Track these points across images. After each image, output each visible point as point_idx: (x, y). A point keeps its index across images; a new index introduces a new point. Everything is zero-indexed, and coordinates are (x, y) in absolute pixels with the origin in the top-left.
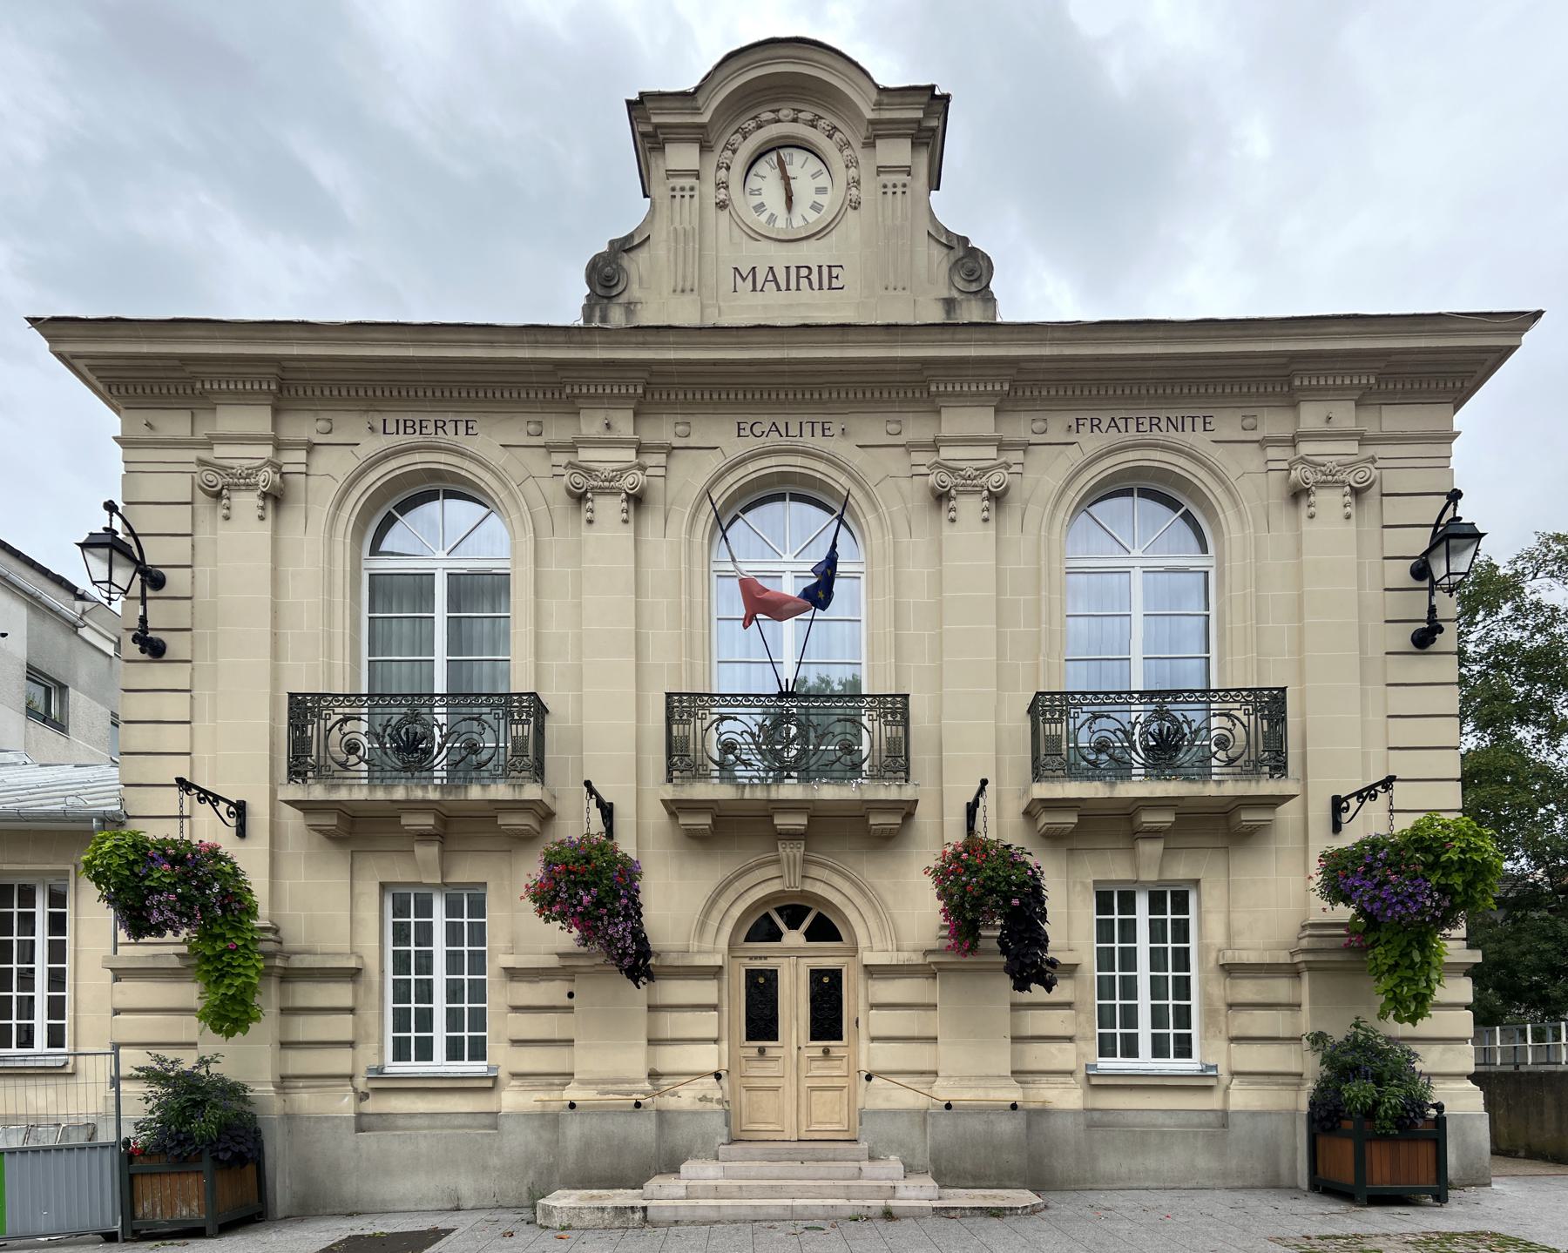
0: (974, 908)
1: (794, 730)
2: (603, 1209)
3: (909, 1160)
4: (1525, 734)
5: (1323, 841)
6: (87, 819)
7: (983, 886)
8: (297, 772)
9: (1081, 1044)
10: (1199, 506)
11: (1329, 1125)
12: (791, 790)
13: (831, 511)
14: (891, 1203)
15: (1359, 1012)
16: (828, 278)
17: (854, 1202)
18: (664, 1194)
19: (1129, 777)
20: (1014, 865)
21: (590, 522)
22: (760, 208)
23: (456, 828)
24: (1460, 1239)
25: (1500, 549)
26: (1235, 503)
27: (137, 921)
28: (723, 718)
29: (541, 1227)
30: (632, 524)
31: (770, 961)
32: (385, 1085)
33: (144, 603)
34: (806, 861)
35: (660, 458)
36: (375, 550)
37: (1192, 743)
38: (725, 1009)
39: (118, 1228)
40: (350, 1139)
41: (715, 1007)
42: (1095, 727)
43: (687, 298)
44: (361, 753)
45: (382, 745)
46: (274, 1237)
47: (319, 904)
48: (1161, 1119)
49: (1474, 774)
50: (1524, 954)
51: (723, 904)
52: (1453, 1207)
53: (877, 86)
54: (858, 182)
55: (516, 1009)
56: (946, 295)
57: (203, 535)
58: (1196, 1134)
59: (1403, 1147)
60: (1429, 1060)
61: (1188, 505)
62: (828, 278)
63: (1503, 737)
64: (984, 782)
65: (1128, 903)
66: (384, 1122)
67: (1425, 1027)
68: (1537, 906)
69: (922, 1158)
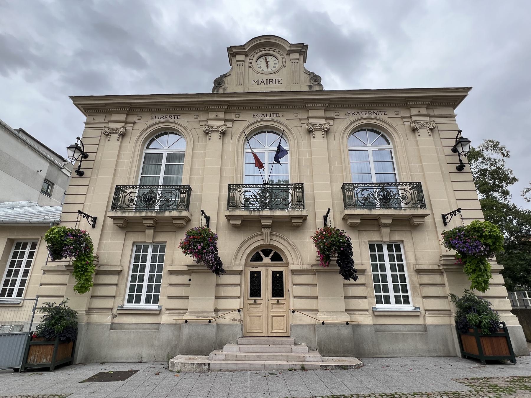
0: (328, 251)
1: (268, 194)
2: (194, 364)
3: (309, 345)
4: (496, 195)
5: (441, 229)
6: (49, 223)
7: (331, 243)
8: (114, 208)
9: (370, 299)
10: (386, 133)
11: (465, 331)
12: (266, 212)
13: (279, 135)
14: (304, 363)
15: (463, 288)
16: (278, 82)
17: (290, 363)
18: (217, 358)
19: (376, 208)
20: (341, 236)
21: (209, 139)
22: (260, 67)
23: (160, 225)
24: (526, 380)
25: (475, 145)
27: (56, 254)
28: (246, 191)
29: (170, 371)
31: (258, 268)
32: (123, 312)
33: (81, 162)
34: (271, 235)
35: (231, 123)
36: (147, 148)
37: (394, 198)
38: (243, 285)
39: (20, 367)
40: (107, 333)
41: (239, 285)
42: (363, 193)
43: (240, 86)
45: (141, 200)
46: (73, 372)
47: (113, 249)
48: (402, 328)
49: (486, 206)
50: (515, 265)
51: (243, 249)
52: (518, 365)
55: (171, 285)
57: (101, 144)
58: (416, 334)
59: (494, 339)
60: (495, 305)
61: (382, 133)
62: (278, 82)
63: (489, 196)
64: (329, 210)
65: (380, 249)
66: (121, 326)
67: (488, 293)
68: (516, 249)
69: (315, 345)
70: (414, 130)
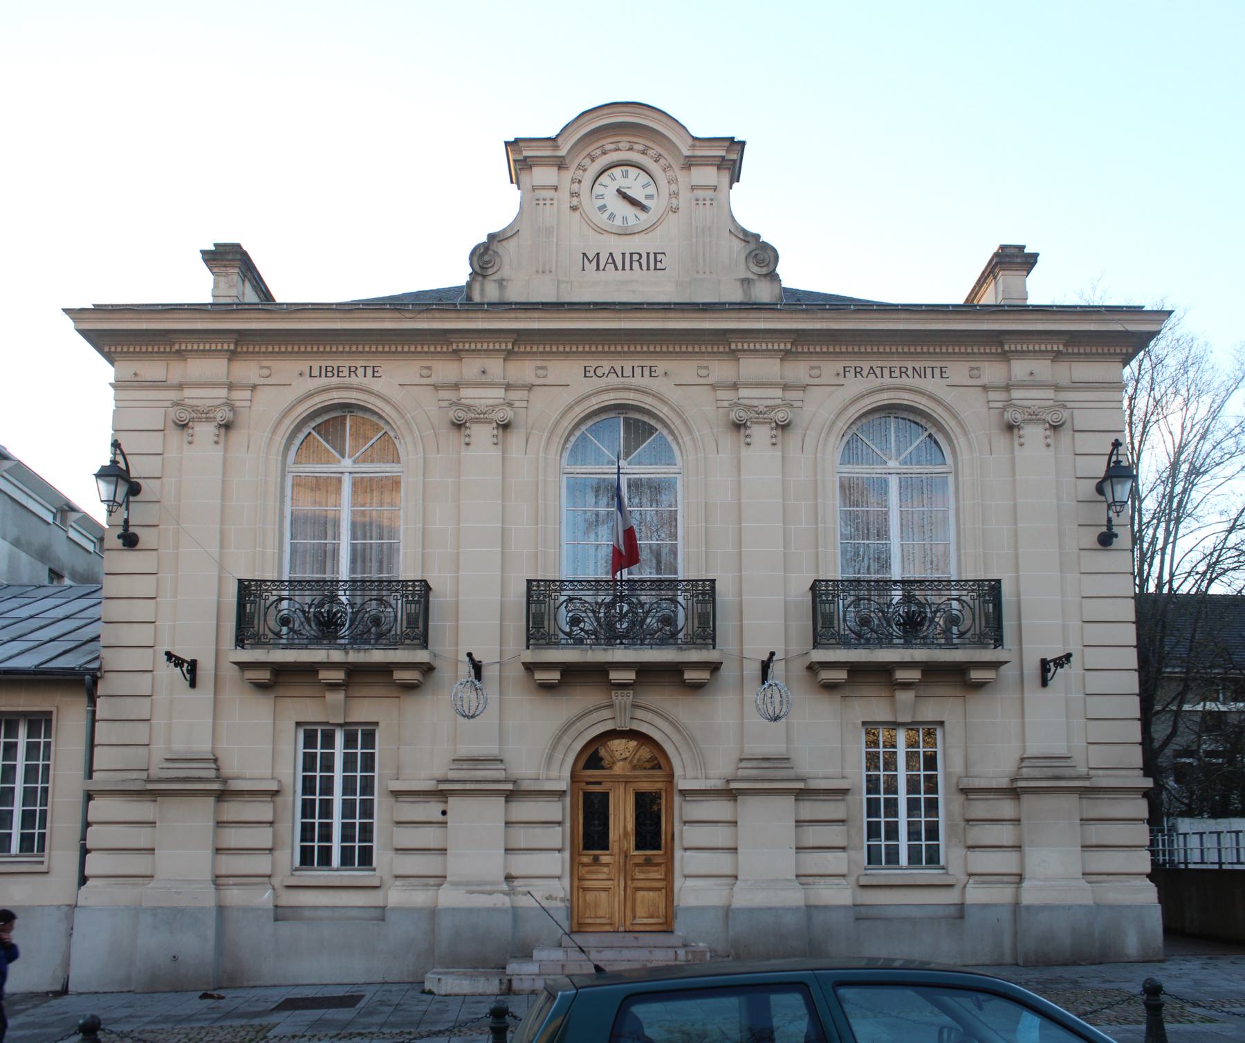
1: (626, 608)
8: (240, 642)
9: (852, 853)
22: (603, 208)
26: (965, 433)
30: (500, 446)
35: (523, 394)
51: (567, 740)
56: (743, 276)
62: (654, 261)
70: (1010, 428)
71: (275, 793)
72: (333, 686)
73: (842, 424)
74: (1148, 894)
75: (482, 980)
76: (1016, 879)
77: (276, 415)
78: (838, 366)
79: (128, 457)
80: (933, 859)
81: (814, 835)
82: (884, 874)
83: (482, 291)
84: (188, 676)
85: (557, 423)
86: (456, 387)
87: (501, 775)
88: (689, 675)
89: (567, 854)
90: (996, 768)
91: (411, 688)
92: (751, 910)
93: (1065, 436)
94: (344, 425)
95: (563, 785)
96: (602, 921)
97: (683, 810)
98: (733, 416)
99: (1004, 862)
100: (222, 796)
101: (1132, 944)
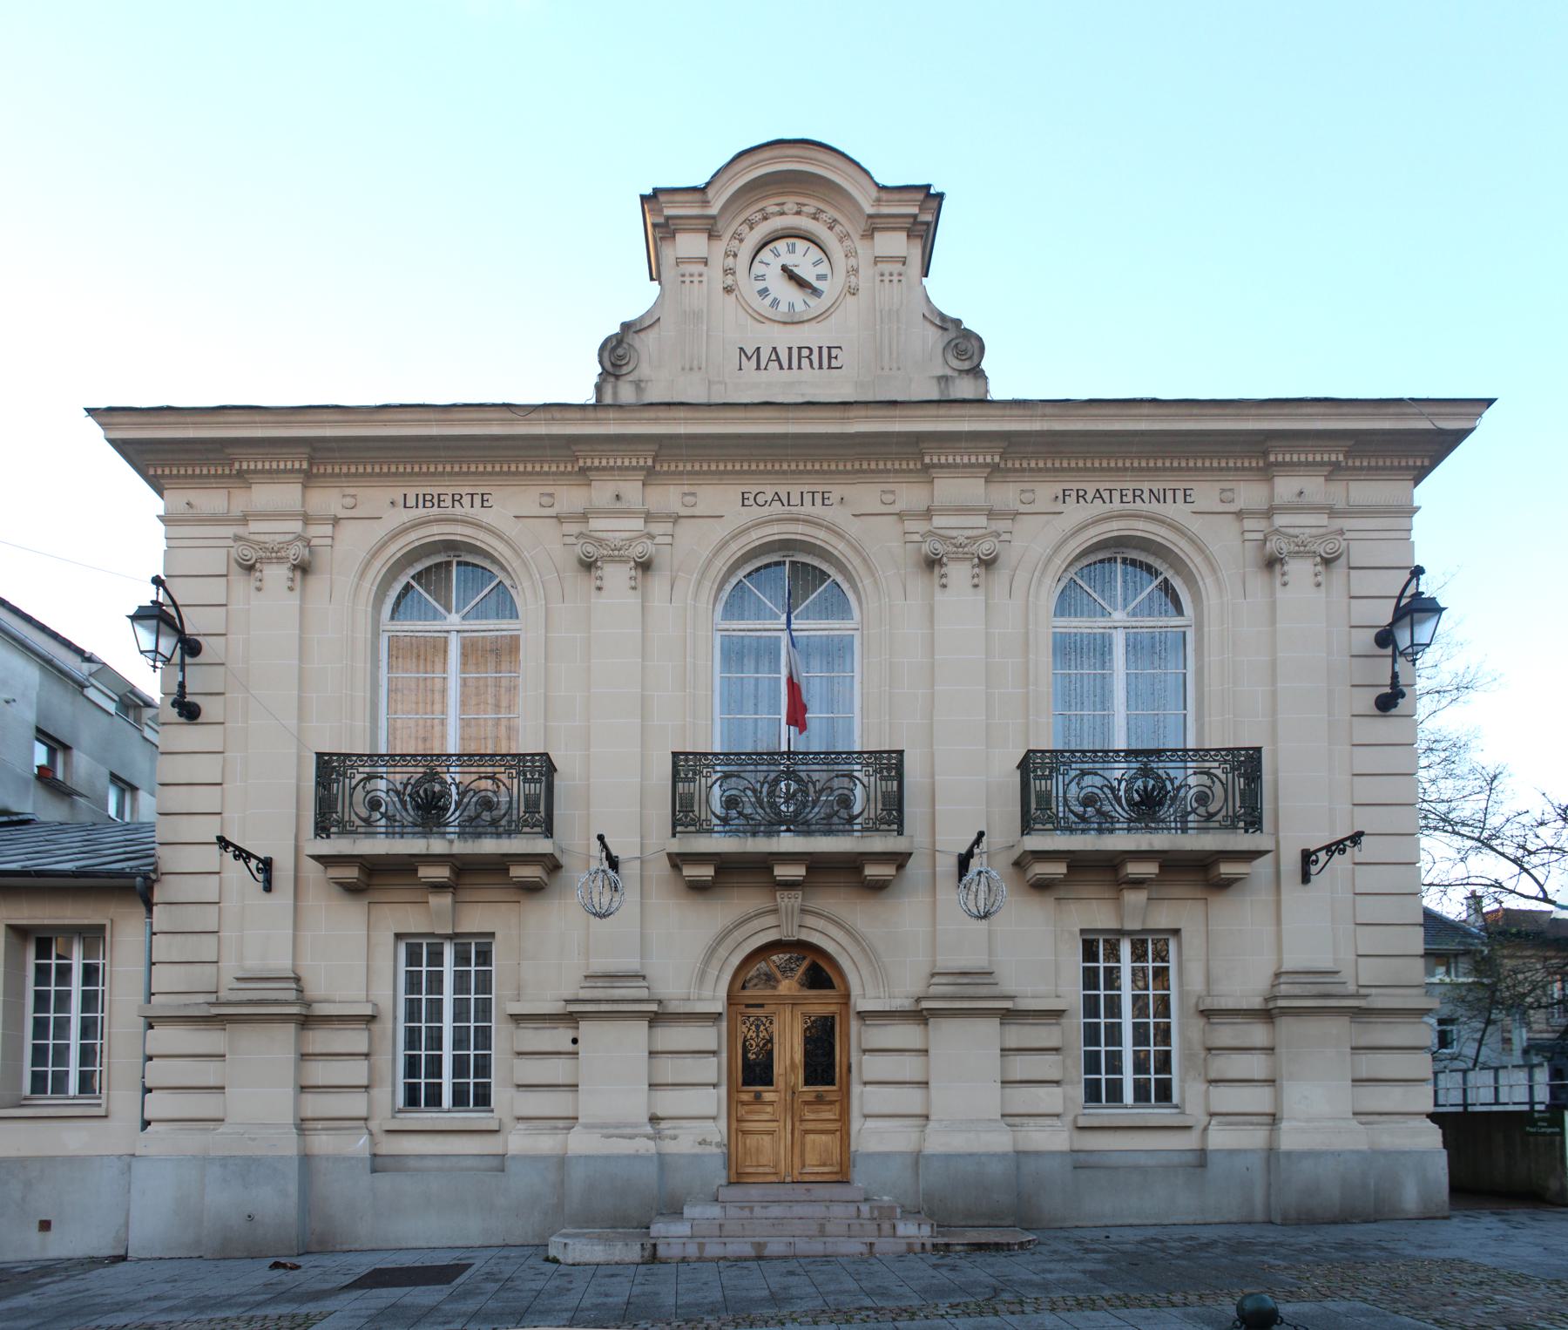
8: (322, 829)
22: (764, 292)
26: (1214, 570)
30: (639, 592)
33: (183, 670)
35: (666, 527)
44: (383, 809)
51: (722, 952)
53: (877, 184)
54: (857, 271)
62: (827, 357)
64: (981, 834)
71: (371, 1019)
72: (438, 887)
73: (1060, 562)
74: (1432, 1137)
75: (620, 1245)
76: (1268, 1119)
77: (362, 555)
78: (1057, 489)
79: (183, 610)
80: (1164, 1092)
81: (1023, 1067)
82: (1105, 1113)
83: (615, 394)
84: (260, 877)
85: (709, 562)
86: (584, 517)
87: (644, 994)
88: (871, 871)
89: (723, 1090)
90: (1245, 984)
91: (532, 889)
92: (948, 1157)
93: (1339, 568)
94: (449, 572)
95: (719, 1006)
96: (767, 1170)
97: (859, 1035)
98: (925, 548)
99: (1256, 1099)
100: (307, 1021)
101: (1410, 1198)
